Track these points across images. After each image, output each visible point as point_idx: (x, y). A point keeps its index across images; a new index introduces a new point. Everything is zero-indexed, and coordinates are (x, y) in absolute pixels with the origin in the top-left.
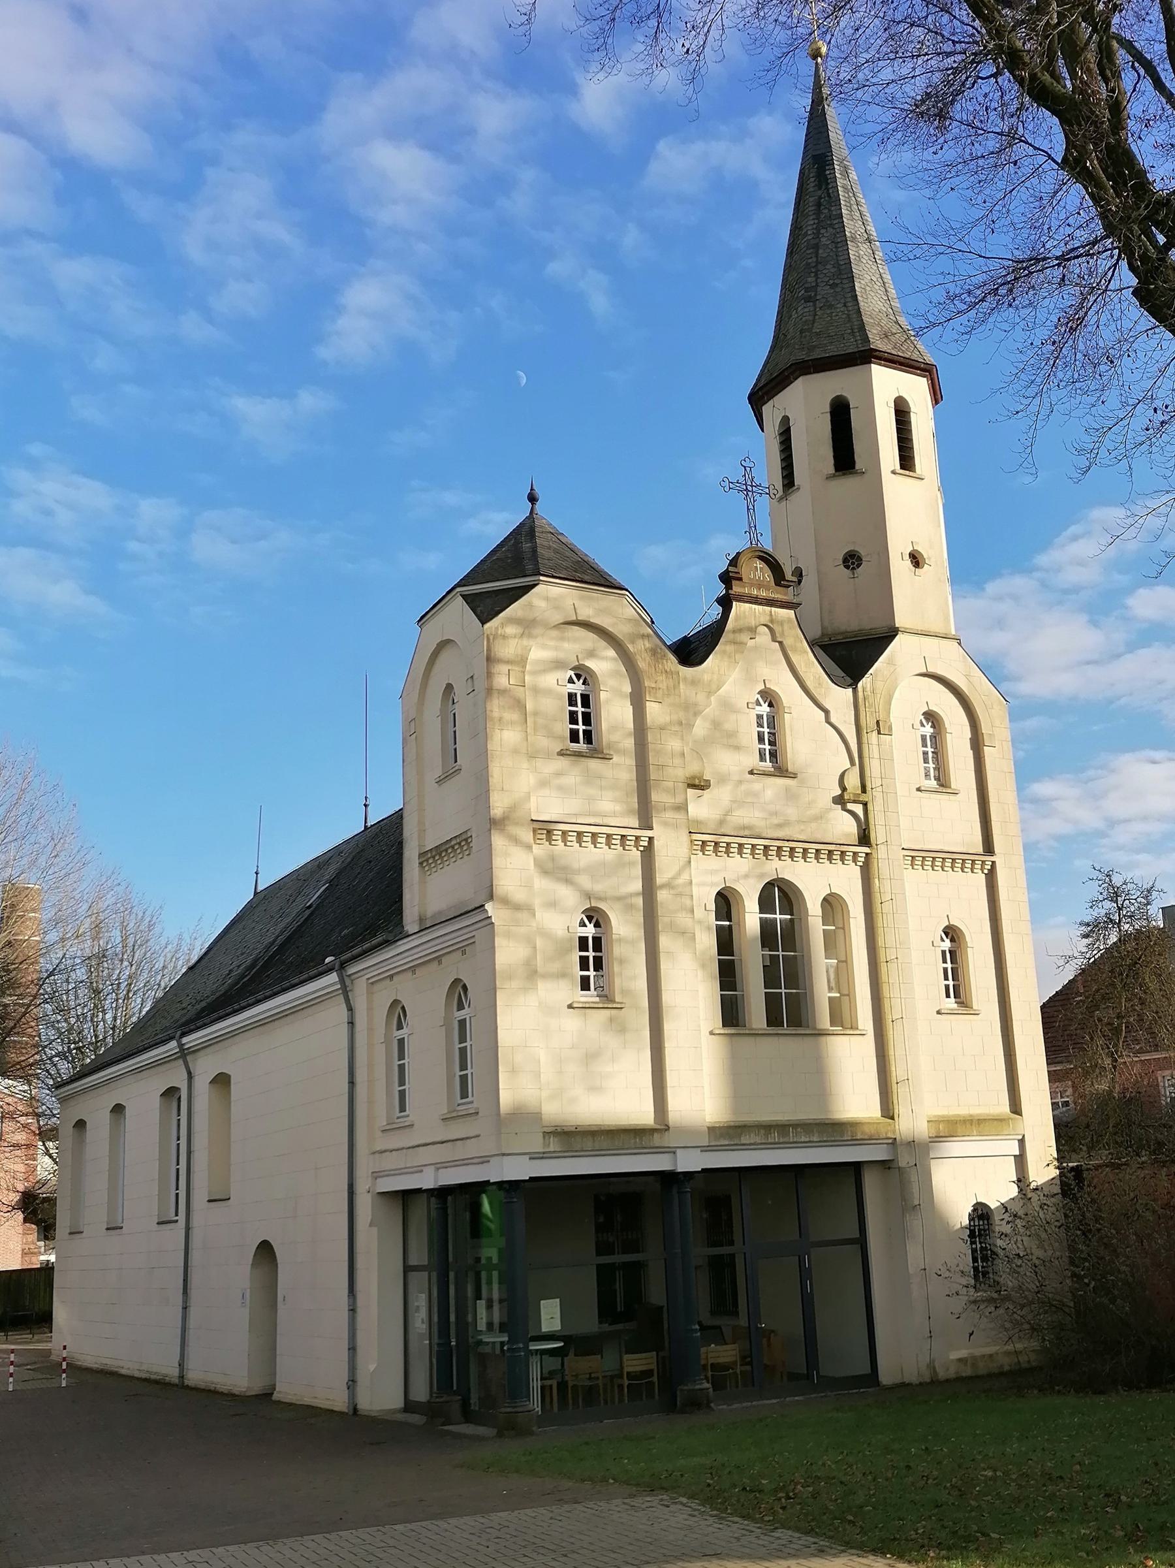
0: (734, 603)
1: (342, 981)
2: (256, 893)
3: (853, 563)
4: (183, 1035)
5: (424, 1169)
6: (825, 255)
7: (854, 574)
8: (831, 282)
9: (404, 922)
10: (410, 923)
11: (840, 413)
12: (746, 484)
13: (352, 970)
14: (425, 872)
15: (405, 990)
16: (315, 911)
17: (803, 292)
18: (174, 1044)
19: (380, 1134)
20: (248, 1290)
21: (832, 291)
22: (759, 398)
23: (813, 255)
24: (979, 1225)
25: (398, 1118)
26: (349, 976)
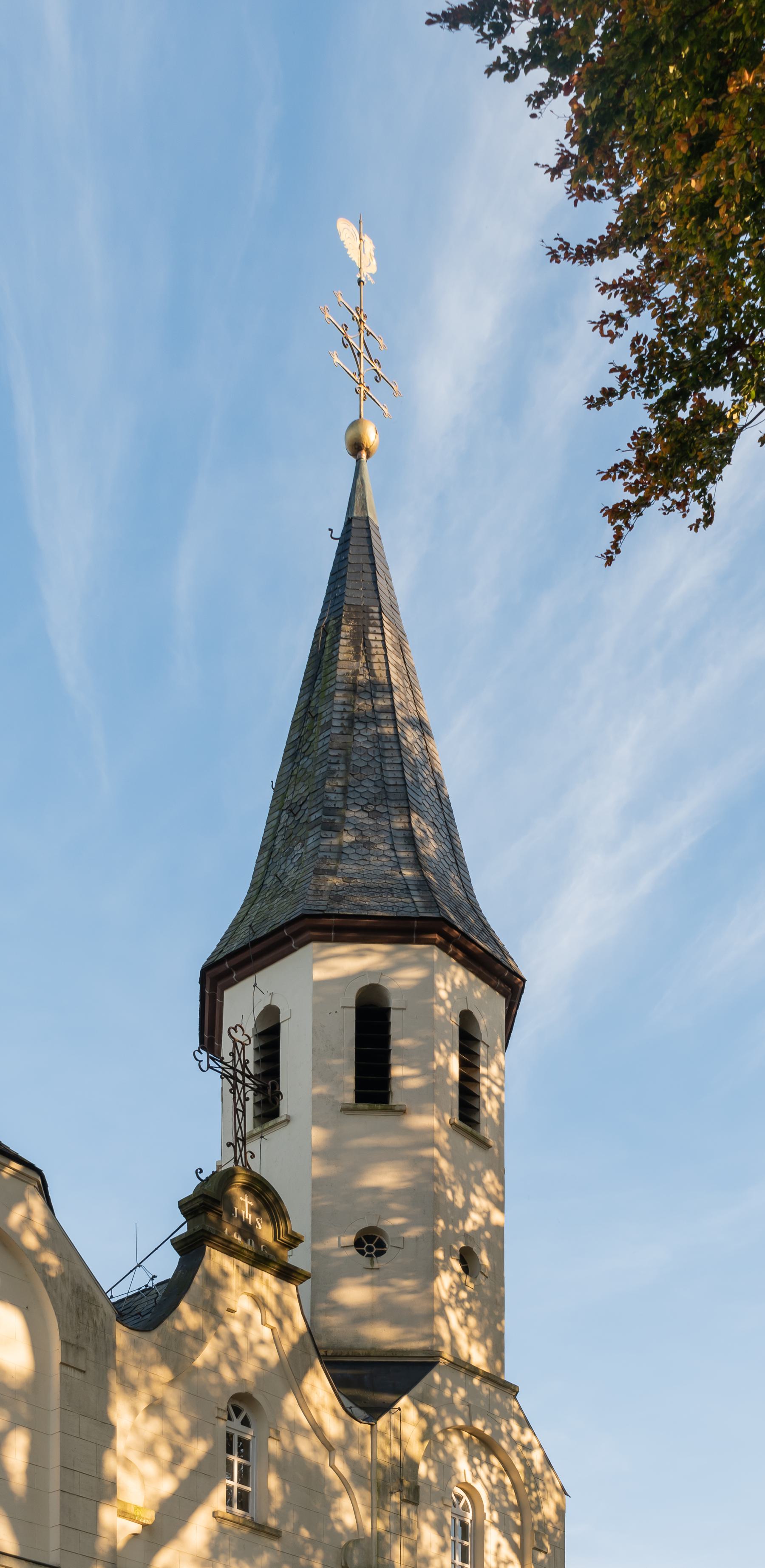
0: (207, 1247)
3: (370, 1249)
7: (372, 1263)
12: (234, 1068)
21: (371, 822)
23: (341, 760)
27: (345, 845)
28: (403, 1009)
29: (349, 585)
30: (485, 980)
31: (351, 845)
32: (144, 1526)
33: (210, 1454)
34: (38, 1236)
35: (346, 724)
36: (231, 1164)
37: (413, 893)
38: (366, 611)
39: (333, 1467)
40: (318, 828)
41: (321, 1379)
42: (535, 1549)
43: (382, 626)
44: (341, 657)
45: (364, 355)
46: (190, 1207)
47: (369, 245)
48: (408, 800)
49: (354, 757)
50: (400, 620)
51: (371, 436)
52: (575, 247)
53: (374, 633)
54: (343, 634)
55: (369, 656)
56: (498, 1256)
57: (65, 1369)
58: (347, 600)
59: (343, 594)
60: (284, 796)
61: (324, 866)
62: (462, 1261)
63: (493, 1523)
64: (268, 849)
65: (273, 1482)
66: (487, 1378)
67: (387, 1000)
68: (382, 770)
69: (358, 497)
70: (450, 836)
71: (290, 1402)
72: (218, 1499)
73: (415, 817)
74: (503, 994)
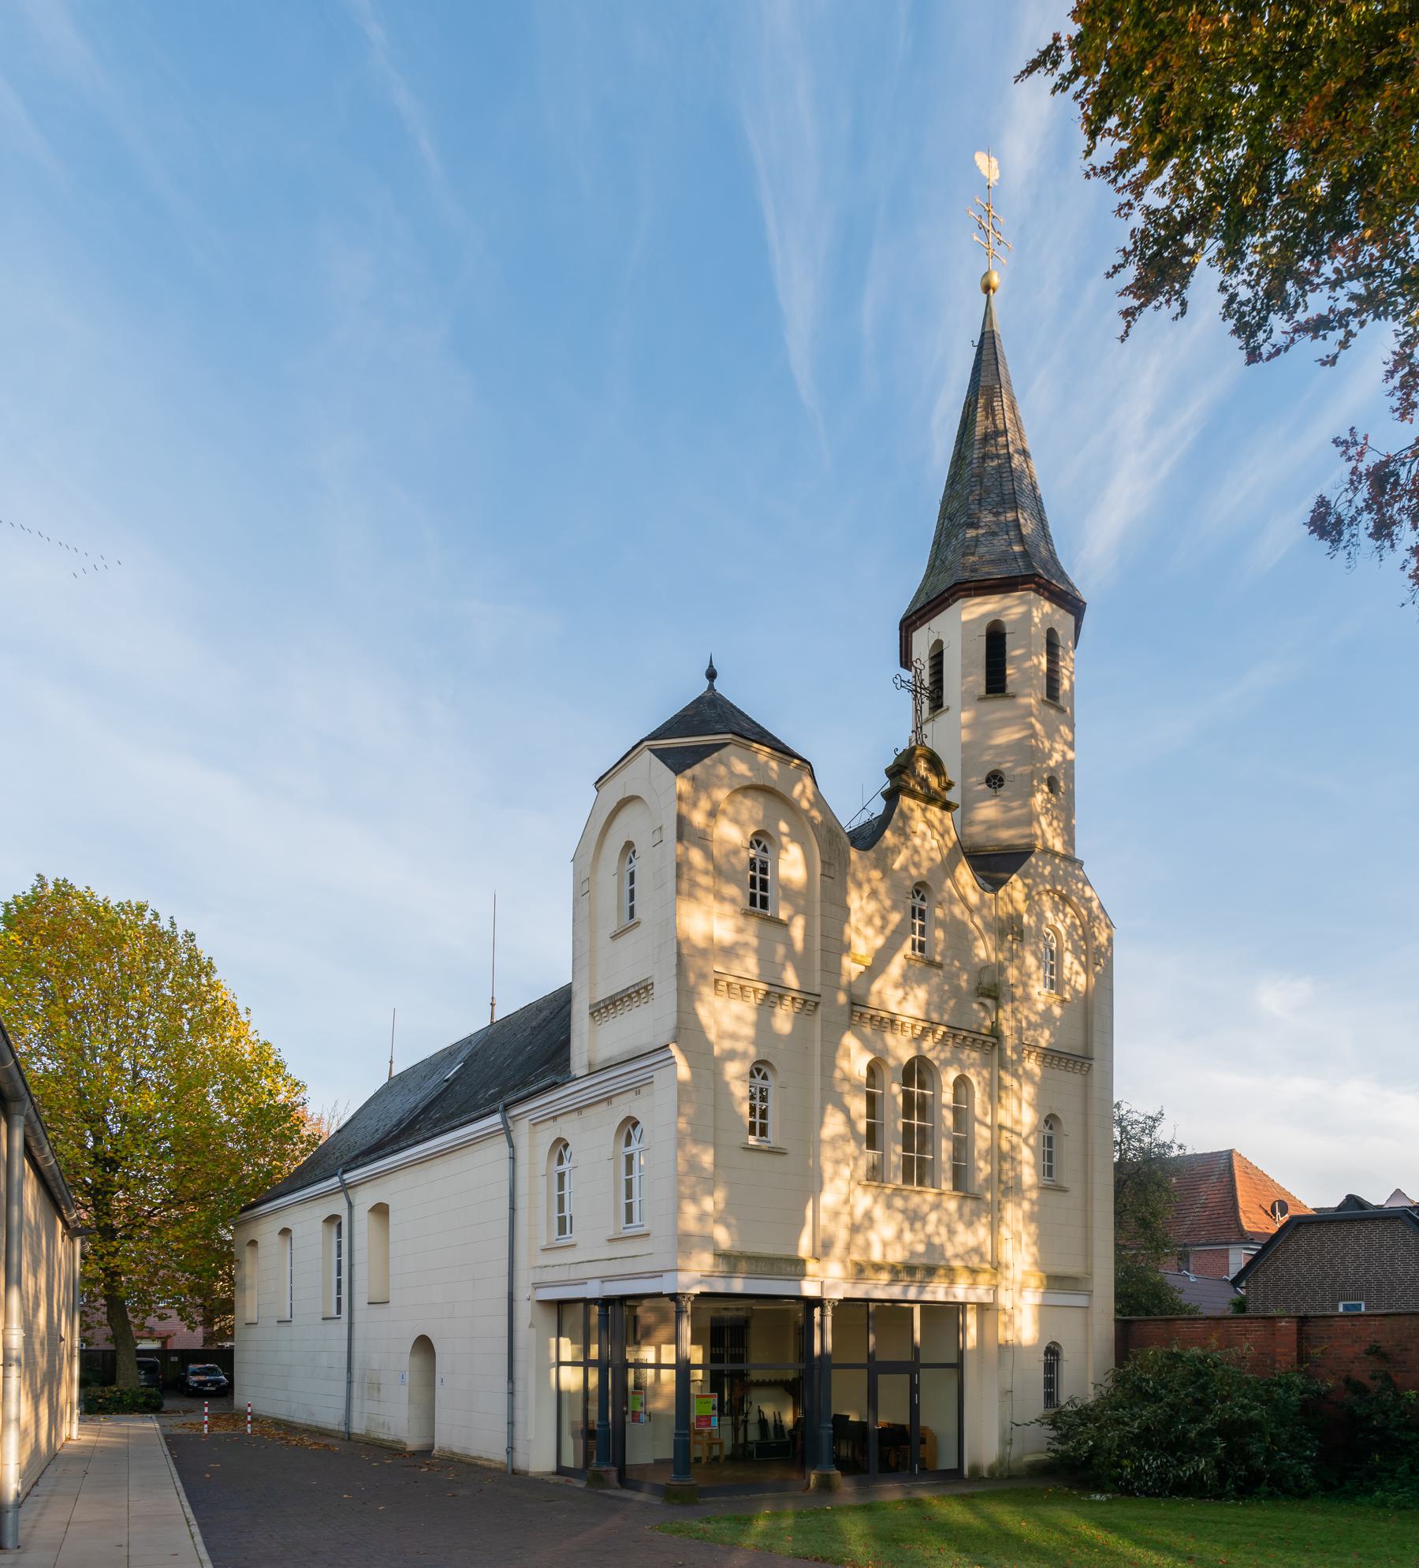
1: (504, 1121)
4: (345, 1172)
5: (589, 1281)
6: (989, 484)
8: (995, 510)
9: (572, 1068)
10: (578, 1066)
11: (996, 639)
12: (915, 685)
13: (515, 1112)
15: (566, 1127)
16: (452, 1083)
18: (336, 1179)
20: (407, 1373)
22: (909, 624)
23: (978, 483)
29: (983, 374)
31: (983, 535)
32: (866, 967)
33: (902, 920)
38: (992, 388)
39: (972, 922)
40: (965, 528)
43: (1001, 396)
44: (978, 419)
45: (992, 231)
49: (985, 480)
51: (995, 279)
55: (994, 416)
58: (981, 384)
65: (939, 934)
67: (1004, 629)
68: (1001, 485)
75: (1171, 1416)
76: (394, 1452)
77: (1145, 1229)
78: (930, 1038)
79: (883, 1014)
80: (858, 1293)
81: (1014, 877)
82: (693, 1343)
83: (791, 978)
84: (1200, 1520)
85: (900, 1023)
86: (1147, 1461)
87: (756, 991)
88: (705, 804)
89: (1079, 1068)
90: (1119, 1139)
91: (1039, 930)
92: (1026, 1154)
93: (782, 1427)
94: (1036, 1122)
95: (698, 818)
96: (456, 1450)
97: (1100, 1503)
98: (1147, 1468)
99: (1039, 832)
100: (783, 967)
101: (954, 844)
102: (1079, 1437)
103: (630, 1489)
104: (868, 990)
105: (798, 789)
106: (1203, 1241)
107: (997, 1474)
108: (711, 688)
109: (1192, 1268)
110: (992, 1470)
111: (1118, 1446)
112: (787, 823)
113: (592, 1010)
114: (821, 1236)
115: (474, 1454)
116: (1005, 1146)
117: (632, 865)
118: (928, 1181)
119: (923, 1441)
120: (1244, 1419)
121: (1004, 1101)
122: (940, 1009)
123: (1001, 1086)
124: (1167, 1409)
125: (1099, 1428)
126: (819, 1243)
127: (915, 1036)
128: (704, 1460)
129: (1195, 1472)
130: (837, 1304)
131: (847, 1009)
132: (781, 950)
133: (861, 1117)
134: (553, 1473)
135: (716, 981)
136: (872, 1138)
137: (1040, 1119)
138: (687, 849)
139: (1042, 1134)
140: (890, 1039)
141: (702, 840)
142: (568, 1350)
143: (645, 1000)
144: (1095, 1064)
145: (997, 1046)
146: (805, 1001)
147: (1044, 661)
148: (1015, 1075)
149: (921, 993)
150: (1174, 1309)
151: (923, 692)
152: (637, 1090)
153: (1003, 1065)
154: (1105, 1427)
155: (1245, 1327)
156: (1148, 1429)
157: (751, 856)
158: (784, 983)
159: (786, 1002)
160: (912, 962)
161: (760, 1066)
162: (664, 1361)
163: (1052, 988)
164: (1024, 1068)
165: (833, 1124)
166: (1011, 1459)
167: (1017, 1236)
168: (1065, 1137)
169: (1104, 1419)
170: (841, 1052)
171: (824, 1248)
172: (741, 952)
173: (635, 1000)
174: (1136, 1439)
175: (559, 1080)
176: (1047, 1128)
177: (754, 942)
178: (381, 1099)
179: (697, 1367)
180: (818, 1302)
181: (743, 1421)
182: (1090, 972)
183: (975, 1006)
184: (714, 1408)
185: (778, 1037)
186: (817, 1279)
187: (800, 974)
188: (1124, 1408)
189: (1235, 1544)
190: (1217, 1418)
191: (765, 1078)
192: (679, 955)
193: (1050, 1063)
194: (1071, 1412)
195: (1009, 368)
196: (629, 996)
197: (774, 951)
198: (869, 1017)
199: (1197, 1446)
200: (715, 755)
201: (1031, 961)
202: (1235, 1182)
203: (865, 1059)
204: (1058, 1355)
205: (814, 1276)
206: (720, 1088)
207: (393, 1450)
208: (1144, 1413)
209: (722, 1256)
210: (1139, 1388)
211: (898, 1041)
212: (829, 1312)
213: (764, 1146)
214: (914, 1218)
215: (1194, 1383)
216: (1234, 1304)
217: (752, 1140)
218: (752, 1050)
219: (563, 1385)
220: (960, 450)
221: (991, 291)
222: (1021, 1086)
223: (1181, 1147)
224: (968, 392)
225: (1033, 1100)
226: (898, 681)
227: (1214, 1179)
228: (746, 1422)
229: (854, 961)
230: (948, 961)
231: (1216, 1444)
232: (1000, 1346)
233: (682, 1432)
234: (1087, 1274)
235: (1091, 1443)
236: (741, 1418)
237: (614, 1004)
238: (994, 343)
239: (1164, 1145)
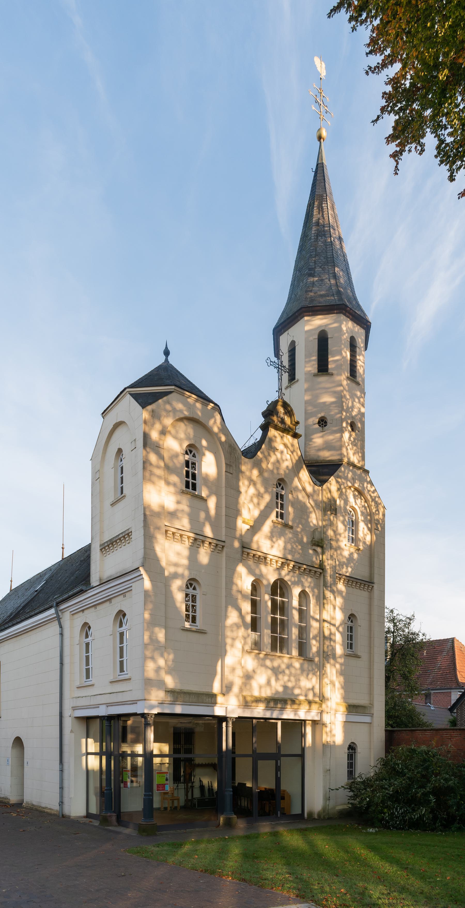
1: (57, 612)
2: (11, 590)
3: (322, 424)
7: (323, 429)
10: (94, 580)
12: (278, 364)
13: (62, 607)
14: (103, 552)
15: (89, 617)
16: (38, 592)
17: (307, 271)
19: (76, 689)
20: (10, 758)
23: (314, 251)
24: (351, 752)
25: (85, 682)
26: (61, 610)
27: (315, 281)
28: (332, 338)
29: (317, 188)
30: (358, 324)
31: (316, 281)
32: (251, 526)
33: (271, 500)
34: (218, 428)
35: (315, 237)
36: (277, 398)
37: (335, 296)
38: (322, 196)
39: (309, 503)
40: (307, 276)
41: (305, 472)
42: (375, 529)
43: (327, 201)
44: (314, 214)
45: (322, 105)
46: (265, 414)
47: (324, 65)
48: (334, 262)
49: (318, 249)
50: (333, 198)
51: (324, 133)
52: (373, 67)
53: (325, 204)
54: (315, 206)
55: (323, 212)
56: (363, 423)
57: (226, 473)
58: (316, 193)
59: (315, 191)
60: (298, 265)
61: (308, 289)
62: (351, 426)
63: (362, 520)
64: (293, 285)
65: (291, 509)
66: (359, 468)
67: (328, 336)
69: (320, 156)
70: (348, 273)
71: (296, 481)
72: (273, 516)
73: (337, 269)
74: (364, 328)
75: (409, 784)
76: (3, 804)
77: (406, 680)
78: (286, 568)
79: (259, 554)
80: (247, 714)
81: (332, 477)
82: (155, 741)
83: (208, 531)
84: (420, 844)
85: (269, 559)
86: (396, 809)
87: (189, 537)
88: (158, 426)
89: (366, 588)
90: (393, 630)
91: (345, 509)
92: (338, 637)
93: (212, 790)
94: (343, 618)
95: (154, 435)
96: (34, 803)
97: (372, 833)
98: (396, 813)
99: (345, 454)
100: (204, 525)
101: (299, 458)
102: (362, 796)
103: (123, 826)
104: (252, 540)
105: (211, 422)
106: (438, 687)
107: (322, 817)
108: (167, 360)
109: (432, 702)
110: (319, 815)
111: (382, 801)
112: (207, 441)
113: (101, 548)
114: (225, 682)
115: (43, 805)
116: (327, 633)
117: (122, 463)
118: (285, 651)
119: (283, 798)
120: (446, 786)
121: (326, 606)
122: (291, 552)
123: (324, 598)
124: (407, 781)
125: (373, 791)
126: (224, 686)
127: (278, 567)
128: (169, 809)
129: (420, 816)
130: (234, 720)
131: (240, 550)
132: (202, 515)
133: (248, 613)
134: (84, 817)
135: (166, 531)
136: (254, 625)
137: (345, 616)
138: (148, 453)
139: (347, 625)
140: (264, 569)
141: (157, 448)
142: (93, 746)
143: (128, 542)
144: (375, 586)
145: (322, 574)
146: (217, 545)
147: (348, 354)
148: (333, 592)
149: (281, 543)
150: (420, 725)
151: (282, 368)
152: (124, 595)
153: (325, 585)
154: (376, 790)
155: (450, 735)
156: (397, 791)
157: (186, 459)
158: (204, 534)
159: (205, 545)
160: (276, 525)
161: (192, 582)
162: (89, 751)
163: (353, 543)
164: (337, 588)
165: (233, 617)
166: (330, 808)
167: (332, 683)
168: (359, 627)
169: (375, 786)
170: (236, 575)
171: (227, 689)
172: (180, 515)
173: (123, 541)
174: (391, 797)
175: (84, 588)
176: (350, 622)
177: (186, 509)
178: (4, 602)
179: (140, 756)
180: (224, 719)
181: (191, 786)
182: (373, 533)
183: (311, 552)
184: (167, 780)
185: (201, 566)
186: (223, 706)
187: (214, 529)
188: (386, 780)
189: (433, 859)
190: (432, 786)
191: (194, 589)
192: (145, 515)
193: (351, 585)
194: (359, 782)
195: (331, 185)
196: (120, 539)
197: (198, 516)
198: (252, 555)
199: (422, 801)
200: (165, 398)
201: (341, 527)
202: (455, 655)
203: (251, 579)
204: (355, 749)
205: (222, 704)
206: (168, 595)
207: (3, 803)
208: (396, 782)
209: (169, 692)
210: (394, 769)
211: (268, 570)
212: (230, 723)
213: (194, 628)
214: (276, 671)
215: (422, 765)
216: (451, 722)
217: (187, 625)
218: (187, 573)
219: (90, 767)
220: (305, 231)
221: (322, 140)
222: (335, 598)
223: (424, 635)
224: (310, 198)
225: (342, 606)
226: (269, 361)
227: (445, 653)
228: (192, 787)
229: (244, 522)
230: (295, 525)
231: (431, 800)
232: (324, 745)
233: (148, 794)
234: (370, 704)
235: (368, 799)
236: (190, 785)
237: (112, 544)
238: (323, 170)
239: (413, 634)
